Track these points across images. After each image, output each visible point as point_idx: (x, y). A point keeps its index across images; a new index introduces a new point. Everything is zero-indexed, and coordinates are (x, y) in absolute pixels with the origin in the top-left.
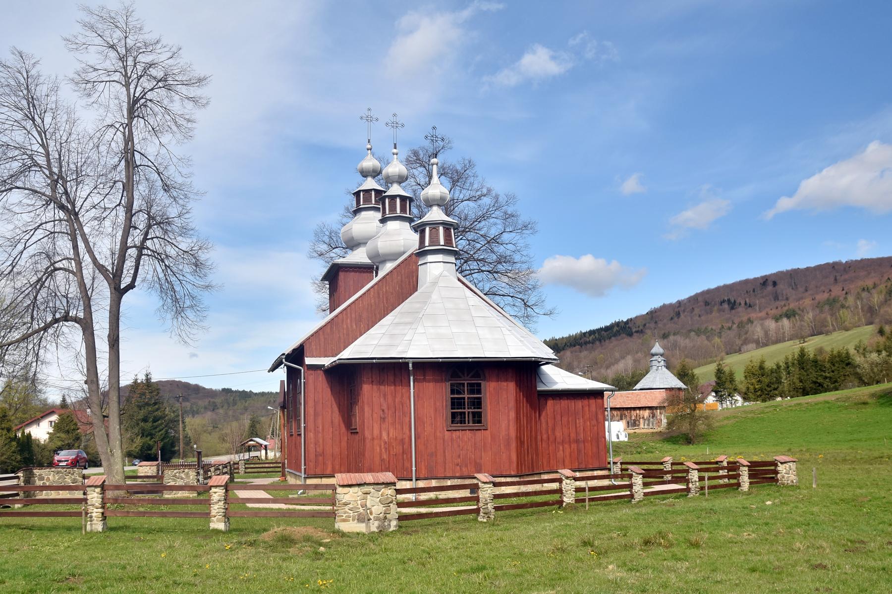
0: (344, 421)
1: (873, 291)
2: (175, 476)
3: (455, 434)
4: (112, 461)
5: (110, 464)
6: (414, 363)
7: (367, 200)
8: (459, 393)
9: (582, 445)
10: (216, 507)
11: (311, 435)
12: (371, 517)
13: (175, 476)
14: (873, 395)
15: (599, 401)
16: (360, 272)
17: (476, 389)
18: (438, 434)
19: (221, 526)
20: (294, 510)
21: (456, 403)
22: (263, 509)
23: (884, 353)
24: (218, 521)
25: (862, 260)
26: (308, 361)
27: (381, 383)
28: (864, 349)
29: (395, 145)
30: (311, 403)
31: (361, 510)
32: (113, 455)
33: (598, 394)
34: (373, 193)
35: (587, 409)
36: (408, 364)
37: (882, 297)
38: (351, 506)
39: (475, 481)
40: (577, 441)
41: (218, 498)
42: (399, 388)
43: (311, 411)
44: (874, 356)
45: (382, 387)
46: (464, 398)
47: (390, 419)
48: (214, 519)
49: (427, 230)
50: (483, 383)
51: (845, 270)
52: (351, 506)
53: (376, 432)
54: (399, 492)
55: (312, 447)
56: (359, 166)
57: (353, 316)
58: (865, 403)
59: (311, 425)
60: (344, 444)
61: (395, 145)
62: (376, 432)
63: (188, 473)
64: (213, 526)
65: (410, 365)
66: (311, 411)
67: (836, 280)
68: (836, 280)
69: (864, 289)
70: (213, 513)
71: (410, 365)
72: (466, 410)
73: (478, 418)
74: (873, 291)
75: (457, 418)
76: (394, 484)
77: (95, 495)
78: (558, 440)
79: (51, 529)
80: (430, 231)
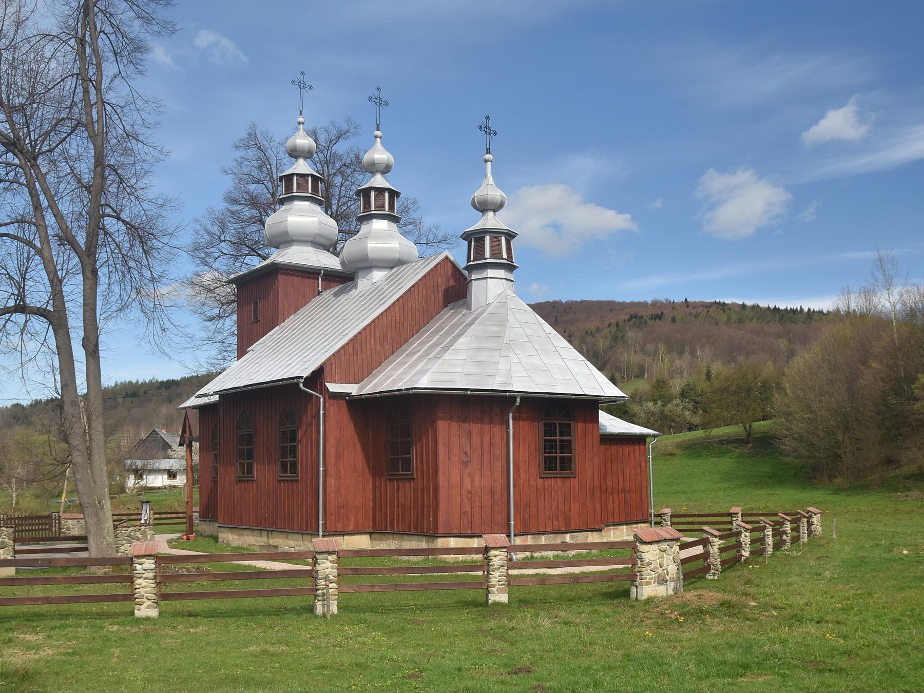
0: (368, 464)
1: (597, 335)
2: (129, 536)
3: (548, 482)
4: (101, 515)
5: (99, 521)
6: (521, 398)
7: (302, 187)
8: (550, 435)
9: (622, 496)
10: (497, 574)
11: (331, 482)
12: (668, 578)
13: (129, 536)
14: (678, 446)
15: (642, 447)
16: (303, 277)
17: (566, 430)
18: (532, 482)
19: (504, 598)
20: (523, 576)
21: (549, 446)
22: (592, 573)
23: (659, 403)
24: (500, 591)
25: (582, 302)
26: (333, 387)
27: (464, 419)
28: (640, 398)
29: (378, 126)
30: (332, 441)
31: (660, 570)
32: (102, 507)
33: (640, 440)
34: (310, 179)
35: (632, 455)
36: (515, 398)
37: (608, 343)
38: (652, 566)
39: (705, 536)
40: (624, 491)
41: (500, 563)
42: (487, 427)
43: (331, 450)
44: (650, 404)
45: (466, 425)
46: (560, 441)
47: (476, 464)
48: (494, 589)
49: (487, 239)
50: (573, 424)
51: (565, 310)
52: (652, 566)
53: (455, 479)
54: (684, 546)
55: (332, 496)
56: (290, 143)
57: (378, 334)
58: (672, 454)
59: (331, 469)
60: (370, 494)
61: (378, 126)
62: (455, 479)
63: (144, 532)
64: (492, 598)
65: (518, 400)
66: (331, 450)
67: (556, 320)
68: (556, 320)
69: (587, 333)
70: (494, 581)
71: (518, 400)
72: (558, 455)
73: (566, 464)
74: (597, 335)
75: (549, 464)
76: (677, 540)
77: (328, 564)
78: (609, 490)
79: (101, 615)
80: (491, 240)
